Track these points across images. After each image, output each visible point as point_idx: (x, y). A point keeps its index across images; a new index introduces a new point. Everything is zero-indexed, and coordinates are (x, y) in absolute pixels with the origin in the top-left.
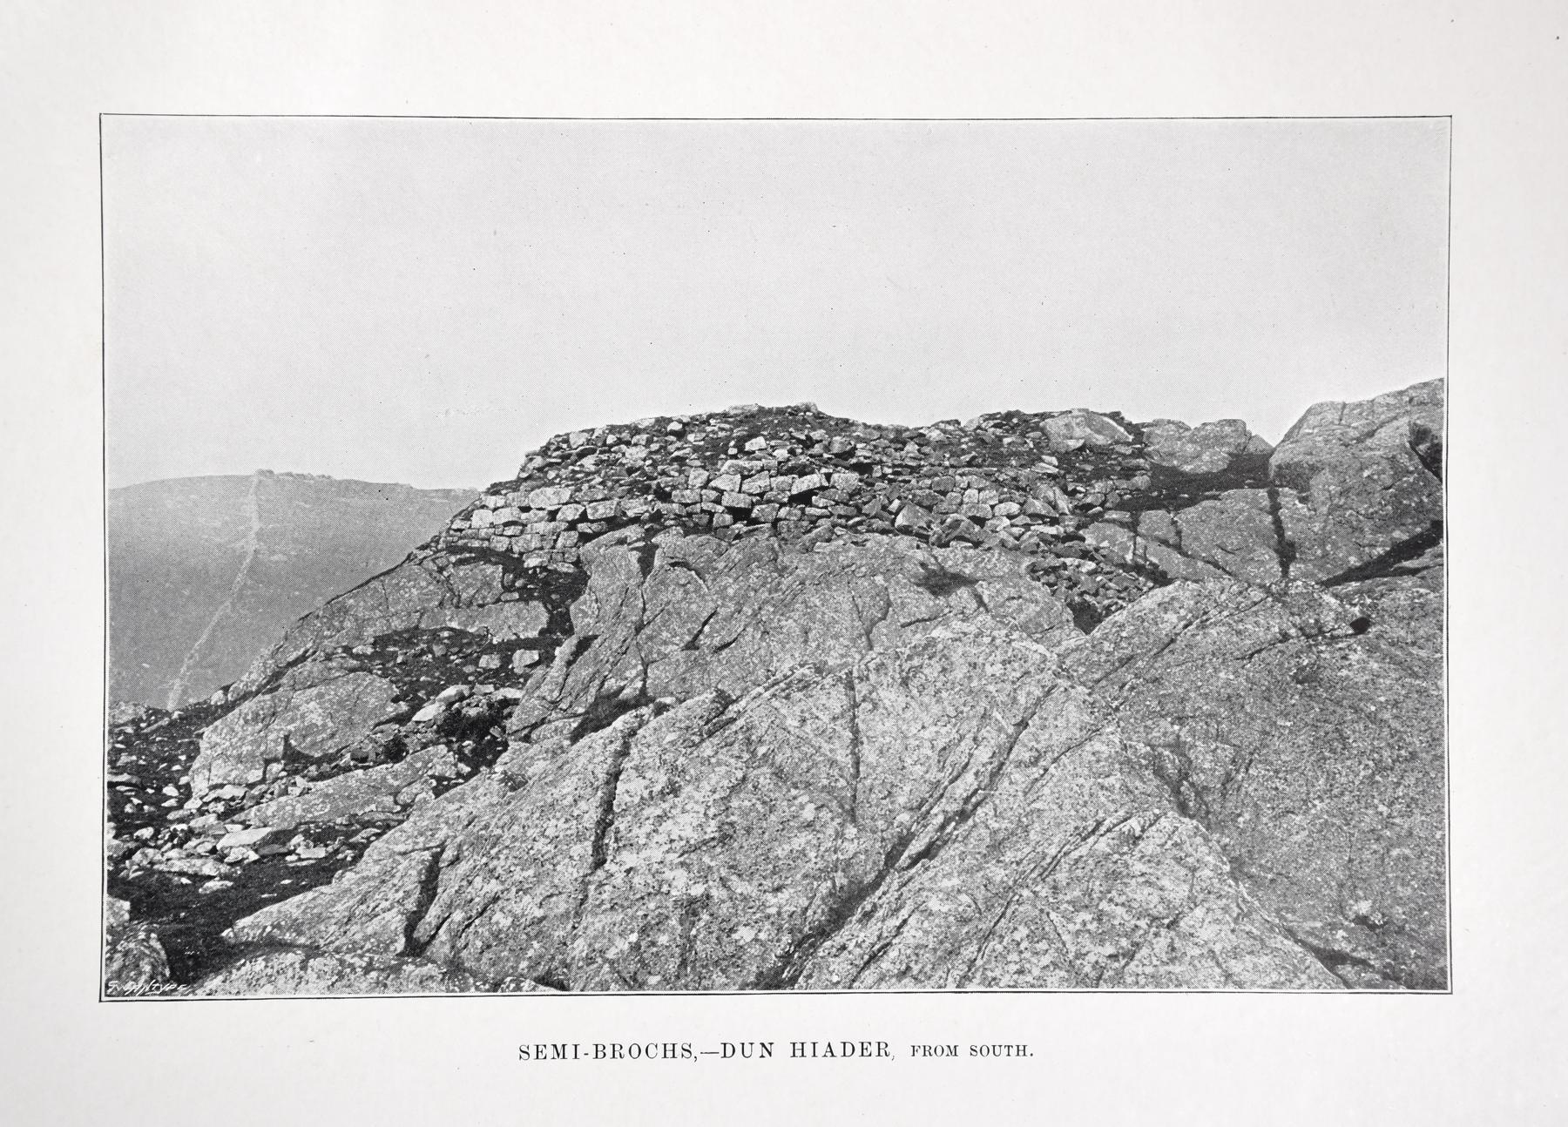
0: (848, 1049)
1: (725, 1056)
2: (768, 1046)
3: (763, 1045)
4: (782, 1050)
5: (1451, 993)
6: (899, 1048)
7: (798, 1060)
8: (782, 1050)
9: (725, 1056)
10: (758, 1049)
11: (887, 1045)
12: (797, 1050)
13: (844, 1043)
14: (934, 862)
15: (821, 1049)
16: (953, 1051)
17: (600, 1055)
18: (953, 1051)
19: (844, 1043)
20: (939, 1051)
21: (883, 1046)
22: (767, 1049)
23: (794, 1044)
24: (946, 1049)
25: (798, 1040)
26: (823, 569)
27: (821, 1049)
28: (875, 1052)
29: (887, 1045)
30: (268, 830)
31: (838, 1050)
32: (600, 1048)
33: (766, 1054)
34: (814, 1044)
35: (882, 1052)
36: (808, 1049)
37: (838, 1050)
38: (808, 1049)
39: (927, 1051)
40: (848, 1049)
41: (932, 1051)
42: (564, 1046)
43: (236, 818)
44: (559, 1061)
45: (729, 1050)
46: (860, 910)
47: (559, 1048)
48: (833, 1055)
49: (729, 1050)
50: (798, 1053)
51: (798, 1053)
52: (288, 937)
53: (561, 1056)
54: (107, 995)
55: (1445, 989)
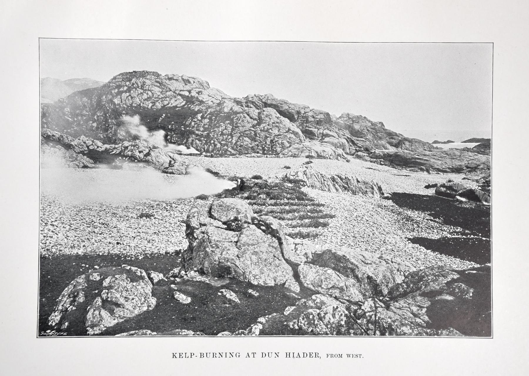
4: (282, 355)
5: (493, 338)
6: (323, 354)
7: (288, 358)
12: (288, 355)
15: (296, 355)
16: (341, 356)
17: (202, 356)
18: (341, 356)
20: (336, 356)
21: (317, 354)
24: (338, 355)
25: (288, 352)
27: (296, 355)
28: (184, 357)
30: (409, 213)
31: (301, 355)
32: (202, 354)
33: (220, 356)
35: (317, 356)
37: (301, 355)
38: (291, 355)
39: (332, 356)
41: (334, 356)
44: (340, 358)
45: (264, 355)
46: (71, 287)
49: (264, 355)
52: (423, 306)
54: (39, 336)
55: (39, 336)
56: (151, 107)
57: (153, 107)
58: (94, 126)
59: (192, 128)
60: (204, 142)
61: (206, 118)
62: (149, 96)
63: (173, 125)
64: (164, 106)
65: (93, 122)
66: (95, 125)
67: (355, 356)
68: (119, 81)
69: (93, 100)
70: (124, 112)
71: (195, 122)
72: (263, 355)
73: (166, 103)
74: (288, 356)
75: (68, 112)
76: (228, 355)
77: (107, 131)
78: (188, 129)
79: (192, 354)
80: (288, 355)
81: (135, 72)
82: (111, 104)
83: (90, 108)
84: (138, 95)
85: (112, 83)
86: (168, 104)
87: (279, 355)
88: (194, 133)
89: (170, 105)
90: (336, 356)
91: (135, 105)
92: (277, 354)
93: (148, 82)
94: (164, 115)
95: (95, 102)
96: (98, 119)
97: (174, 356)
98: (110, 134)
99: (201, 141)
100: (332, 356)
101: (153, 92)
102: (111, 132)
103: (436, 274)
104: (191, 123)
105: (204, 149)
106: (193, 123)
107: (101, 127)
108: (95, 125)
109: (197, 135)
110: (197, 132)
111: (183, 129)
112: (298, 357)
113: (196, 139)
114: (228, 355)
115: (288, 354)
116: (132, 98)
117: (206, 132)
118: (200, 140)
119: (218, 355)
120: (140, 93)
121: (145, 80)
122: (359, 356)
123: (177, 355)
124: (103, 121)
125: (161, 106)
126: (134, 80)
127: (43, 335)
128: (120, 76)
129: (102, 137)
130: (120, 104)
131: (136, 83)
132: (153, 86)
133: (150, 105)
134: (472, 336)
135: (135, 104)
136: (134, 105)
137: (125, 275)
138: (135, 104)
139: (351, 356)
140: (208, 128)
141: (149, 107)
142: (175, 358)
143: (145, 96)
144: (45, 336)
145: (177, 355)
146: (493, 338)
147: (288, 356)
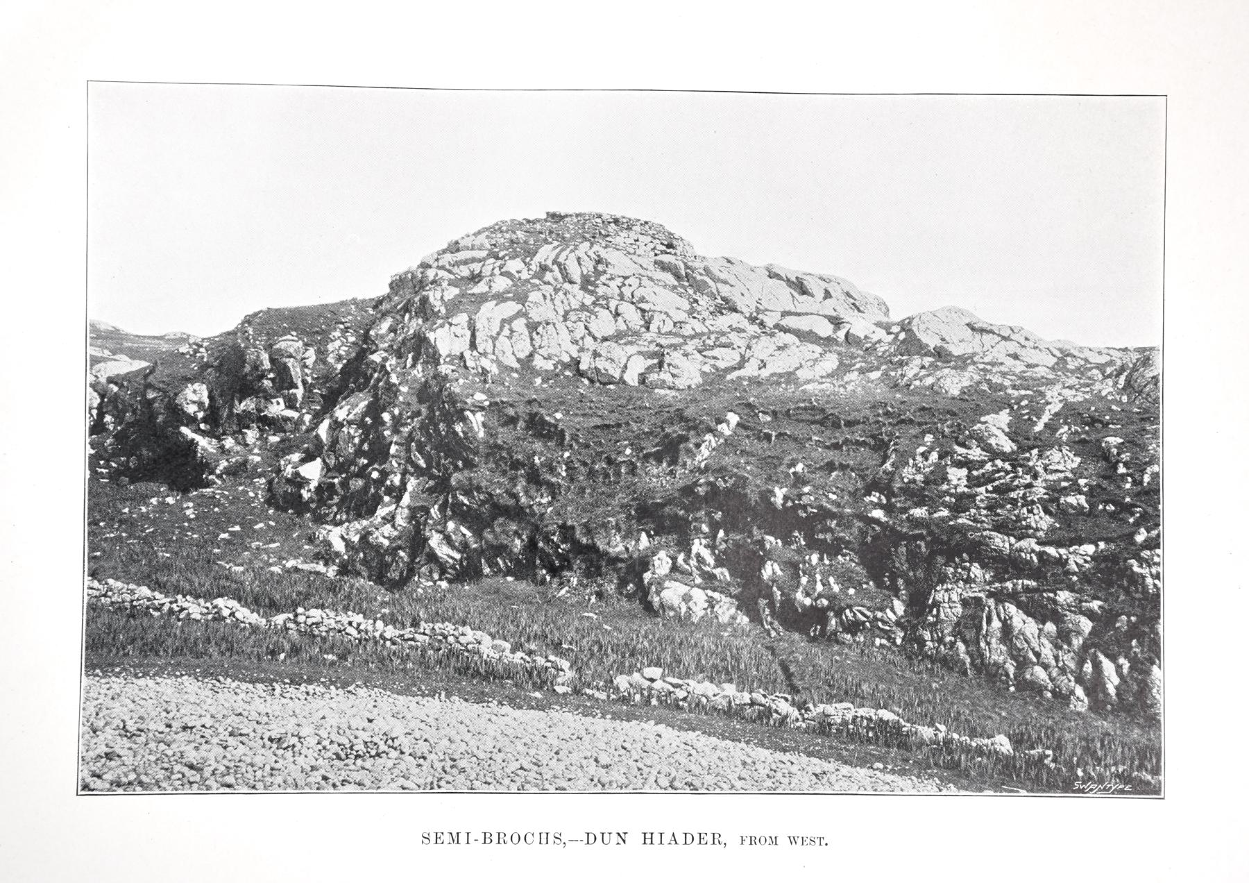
4: (635, 839)
6: (731, 837)
7: (648, 846)
18: (774, 841)
20: (763, 840)
21: (717, 836)
24: (768, 839)
25: (648, 831)
31: (680, 839)
35: (716, 841)
37: (680, 839)
38: (656, 838)
39: (753, 841)
41: (757, 841)
44: (773, 846)
56: (643, 379)
57: (653, 377)
58: (307, 482)
59: (957, 509)
60: (1086, 625)
61: (1044, 443)
62: (623, 327)
63: (799, 481)
64: (721, 374)
65: (309, 457)
66: (313, 471)
67: (808, 841)
68: (474, 260)
69: (330, 347)
70: (480, 396)
71: (965, 463)
73: (727, 358)
74: (648, 841)
75: (200, 404)
77: (372, 512)
78: (919, 512)
81: (555, 217)
82: (415, 360)
83: (308, 388)
84: (565, 318)
85: (439, 268)
86: (740, 366)
87: (627, 838)
88: (979, 552)
89: (750, 370)
90: (763, 840)
91: (549, 366)
92: (623, 835)
93: (619, 263)
94: (733, 418)
95: (339, 358)
96: (335, 442)
98: (387, 529)
99: (1057, 618)
100: (753, 841)
101: (643, 306)
102: (390, 519)
104: (939, 476)
105: (1095, 687)
106: (957, 476)
107: (344, 484)
108: (313, 471)
109: (1006, 565)
110: (1001, 542)
111: (878, 514)
112: (673, 842)
113: (1000, 597)
115: (648, 836)
116: (533, 327)
117: (1089, 549)
118: (1041, 611)
120: (575, 304)
121: (603, 253)
122: (817, 841)
124: (359, 452)
125: (703, 374)
126: (545, 254)
128: (482, 239)
129: (339, 546)
130: (462, 357)
131: (555, 262)
132: (645, 281)
133: (638, 366)
135: (549, 358)
136: (539, 362)
138: (549, 358)
139: (799, 841)
140: (1092, 514)
141: (632, 378)
143: (604, 324)
147: (648, 841)
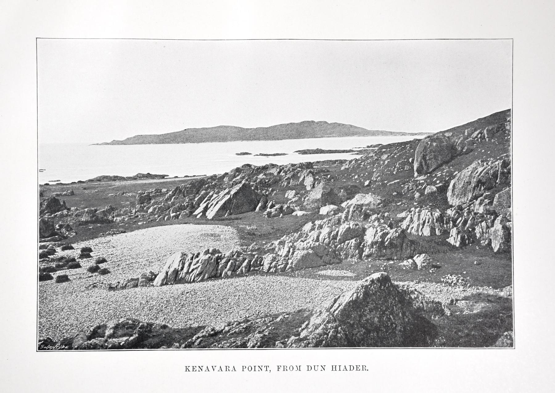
0: (352, 368)
1: (350, 370)
2: (201, 367)
3: (199, 367)
4: (328, 368)
5: (37, 351)
6: (239, 368)
7: (334, 372)
8: (328, 368)
9: (350, 370)
10: (320, 368)
11: (229, 367)
12: (334, 368)
13: (350, 366)
14: (62, 255)
15: (342, 368)
16: (299, 368)
18: (299, 368)
19: (350, 366)
22: (323, 368)
23: (278, 366)
25: (334, 365)
26: (449, 221)
27: (342, 368)
29: (229, 367)
31: (348, 368)
34: (340, 366)
36: (338, 368)
37: (348, 368)
38: (338, 368)
40: (352, 368)
42: (300, 366)
43: (471, 172)
45: (310, 368)
47: (187, 370)
48: (346, 370)
49: (310, 368)
50: (334, 369)
51: (334, 369)
53: (299, 370)
72: (309, 368)
76: (257, 368)
79: (244, 367)
80: (334, 368)
87: (325, 368)
97: (187, 369)
103: (293, 233)
114: (257, 368)
119: (197, 369)
123: (191, 369)
127: (43, 349)
134: (410, 347)
137: (438, 210)
142: (188, 372)
144: (45, 349)
145: (191, 369)
146: (37, 351)
